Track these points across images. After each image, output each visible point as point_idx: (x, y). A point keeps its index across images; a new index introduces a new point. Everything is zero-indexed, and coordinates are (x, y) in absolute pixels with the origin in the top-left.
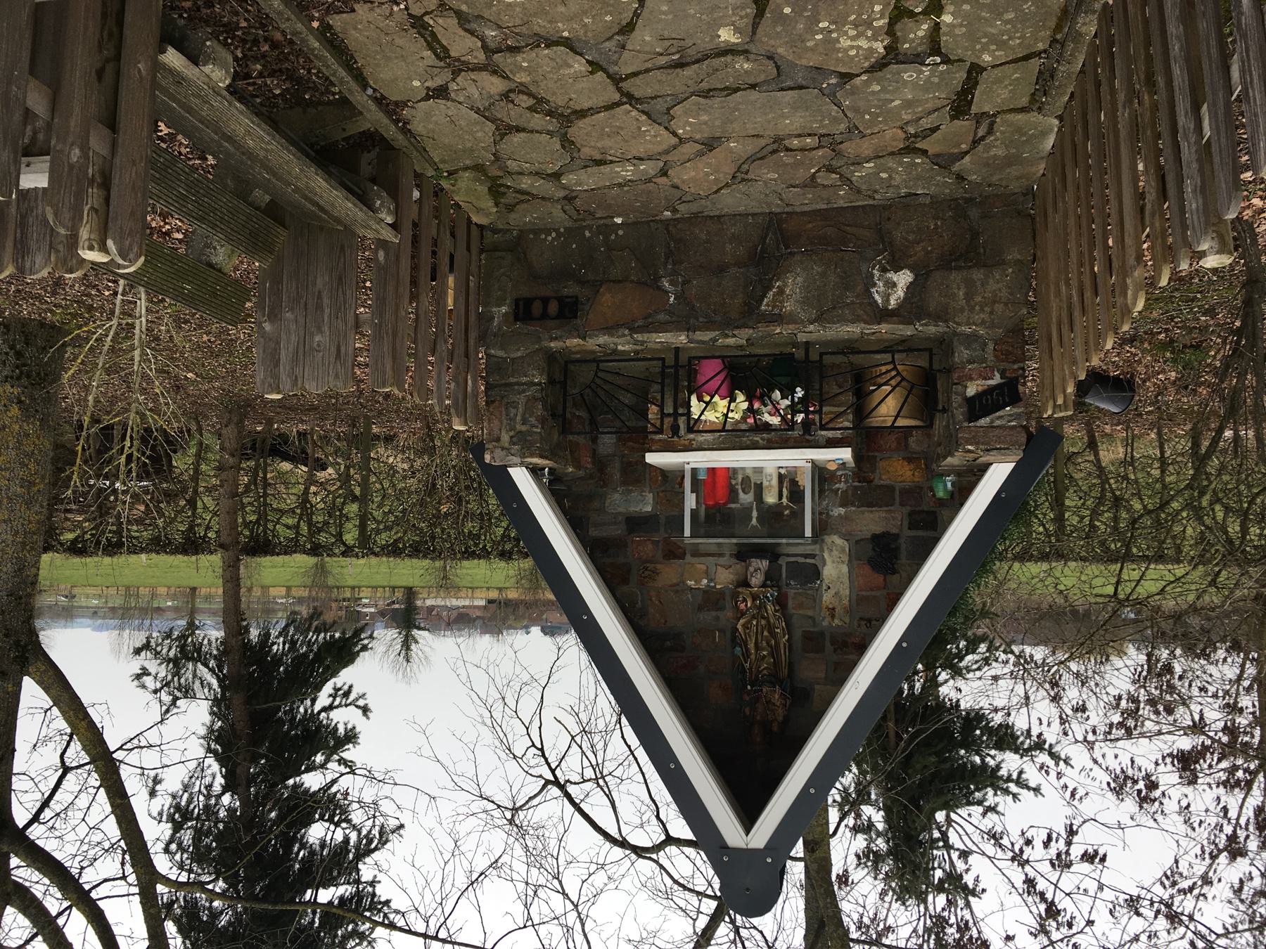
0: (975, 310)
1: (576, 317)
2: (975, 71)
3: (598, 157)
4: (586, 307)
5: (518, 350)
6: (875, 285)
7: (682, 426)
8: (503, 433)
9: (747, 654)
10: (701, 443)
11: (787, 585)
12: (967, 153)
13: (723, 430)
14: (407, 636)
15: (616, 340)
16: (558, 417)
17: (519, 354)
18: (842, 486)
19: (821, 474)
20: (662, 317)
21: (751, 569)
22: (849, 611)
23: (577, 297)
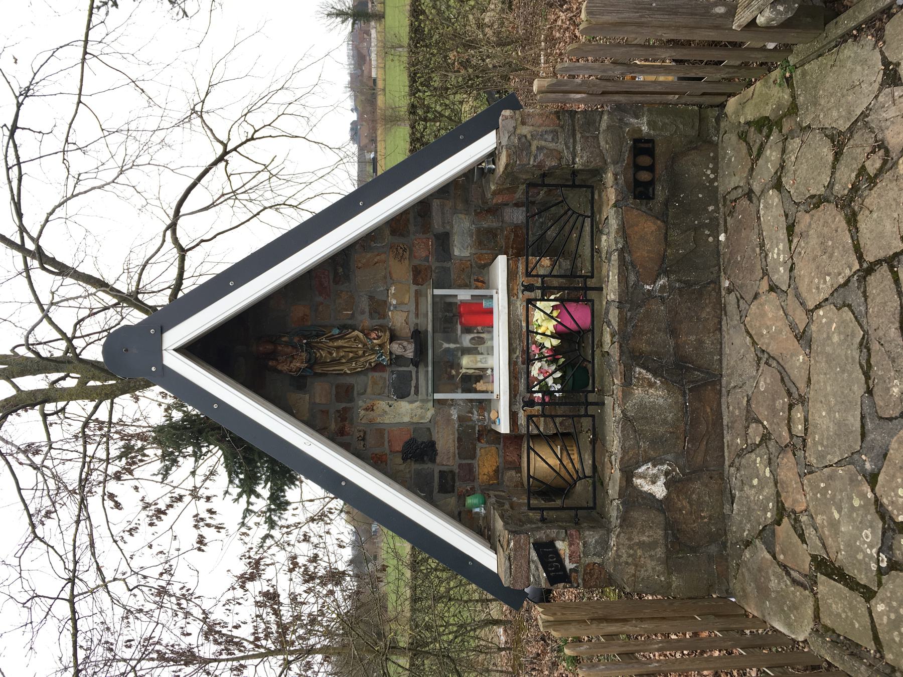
0: (625, 548)
1: (635, 198)
2: (868, 594)
3: (797, 229)
4: (644, 208)
5: (607, 143)
6: (654, 466)
7: (532, 295)
8: (531, 128)
9: (332, 339)
10: (514, 304)
11: (392, 372)
12: (774, 557)
13: (529, 332)
14: (347, 14)
15: (613, 235)
16: (542, 179)
17: (602, 143)
18: (475, 417)
19: (485, 405)
20: (632, 278)
21: (405, 344)
22: (371, 422)
23: (653, 198)
